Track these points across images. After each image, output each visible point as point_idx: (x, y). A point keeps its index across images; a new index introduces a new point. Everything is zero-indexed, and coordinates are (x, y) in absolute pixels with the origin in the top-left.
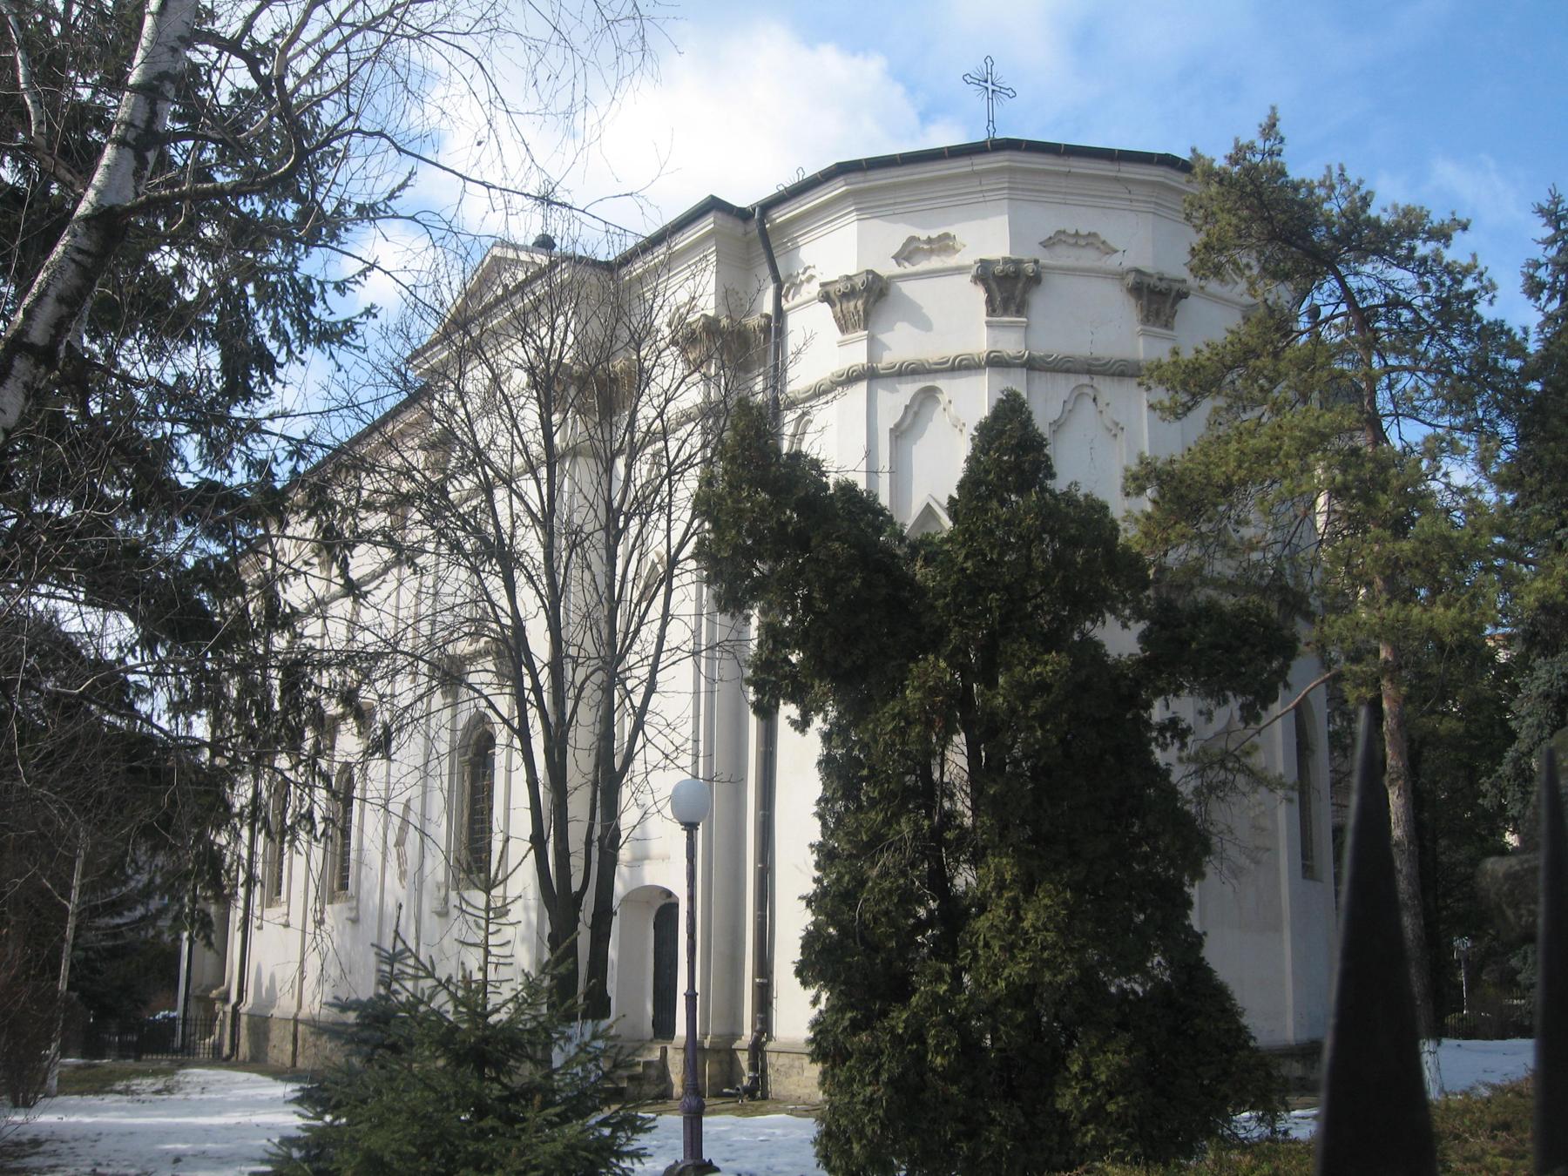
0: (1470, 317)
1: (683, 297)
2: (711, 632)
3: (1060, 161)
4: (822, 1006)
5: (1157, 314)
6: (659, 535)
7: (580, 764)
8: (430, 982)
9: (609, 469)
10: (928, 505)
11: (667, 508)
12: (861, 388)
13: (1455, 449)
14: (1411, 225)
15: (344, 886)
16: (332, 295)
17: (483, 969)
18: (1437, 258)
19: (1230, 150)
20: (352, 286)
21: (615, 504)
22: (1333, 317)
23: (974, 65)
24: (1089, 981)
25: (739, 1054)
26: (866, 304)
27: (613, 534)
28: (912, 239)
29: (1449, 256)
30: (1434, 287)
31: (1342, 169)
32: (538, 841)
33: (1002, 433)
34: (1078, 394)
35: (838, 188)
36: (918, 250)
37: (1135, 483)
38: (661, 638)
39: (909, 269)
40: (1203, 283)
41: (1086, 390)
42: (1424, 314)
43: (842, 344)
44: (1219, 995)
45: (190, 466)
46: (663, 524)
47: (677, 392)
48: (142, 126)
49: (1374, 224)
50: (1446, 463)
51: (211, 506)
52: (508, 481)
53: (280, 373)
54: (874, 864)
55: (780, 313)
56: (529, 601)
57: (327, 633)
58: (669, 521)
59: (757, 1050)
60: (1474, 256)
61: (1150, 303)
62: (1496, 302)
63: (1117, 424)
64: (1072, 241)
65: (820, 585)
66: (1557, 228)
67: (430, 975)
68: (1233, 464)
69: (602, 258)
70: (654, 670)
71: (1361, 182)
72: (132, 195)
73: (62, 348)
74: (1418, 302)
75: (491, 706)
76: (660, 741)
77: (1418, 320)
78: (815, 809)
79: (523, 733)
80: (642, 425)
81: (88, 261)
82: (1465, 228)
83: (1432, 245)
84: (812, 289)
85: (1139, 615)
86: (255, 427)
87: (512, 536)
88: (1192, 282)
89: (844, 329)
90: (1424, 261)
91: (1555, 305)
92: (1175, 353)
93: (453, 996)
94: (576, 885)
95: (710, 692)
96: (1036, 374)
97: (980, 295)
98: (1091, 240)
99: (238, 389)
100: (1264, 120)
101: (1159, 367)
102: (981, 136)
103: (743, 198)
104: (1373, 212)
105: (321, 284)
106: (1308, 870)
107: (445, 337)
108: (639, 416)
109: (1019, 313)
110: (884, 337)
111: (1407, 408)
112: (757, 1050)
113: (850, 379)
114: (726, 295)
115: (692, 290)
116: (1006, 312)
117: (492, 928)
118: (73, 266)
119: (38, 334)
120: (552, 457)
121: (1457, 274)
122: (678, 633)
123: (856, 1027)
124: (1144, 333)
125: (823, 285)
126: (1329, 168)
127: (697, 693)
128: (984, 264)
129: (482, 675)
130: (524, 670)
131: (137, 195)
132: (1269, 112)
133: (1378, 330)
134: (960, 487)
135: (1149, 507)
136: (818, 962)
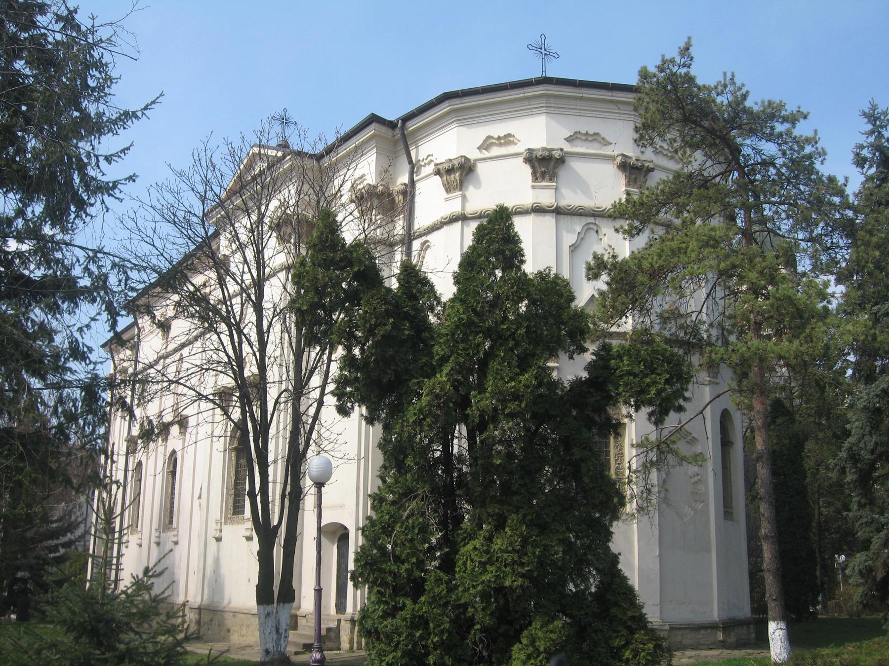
0: (811, 170)
3: (577, 90)
12: (458, 225)
14: (773, 112)
15: (171, 522)
16: (103, 163)
18: (789, 133)
19: (659, 62)
20: (116, 158)
23: (535, 39)
26: (461, 175)
28: (489, 137)
29: (796, 132)
31: (733, 75)
34: (587, 228)
35: (445, 108)
36: (492, 144)
39: (486, 154)
41: (592, 226)
42: (783, 170)
43: (447, 200)
49: (749, 112)
53: (89, 210)
55: (412, 183)
60: (816, 131)
61: (631, 174)
62: (825, 162)
64: (584, 138)
66: (874, 125)
71: (743, 85)
77: (779, 174)
78: (378, 473)
82: (805, 117)
83: (787, 126)
84: (431, 168)
89: (448, 190)
90: (780, 135)
91: (873, 170)
96: (562, 216)
97: (527, 170)
98: (594, 137)
100: (682, 45)
103: (391, 116)
104: (748, 103)
106: (727, 511)
109: (551, 180)
110: (467, 194)
115: (366, 169)
116: (543, 179)
121: (801, 143)
123: (385, 615)
125: (436, 165)
126: (725, 74)
128: (530, 151)
132: (686, 40)
134: (460, 265)
135: (605, 288)
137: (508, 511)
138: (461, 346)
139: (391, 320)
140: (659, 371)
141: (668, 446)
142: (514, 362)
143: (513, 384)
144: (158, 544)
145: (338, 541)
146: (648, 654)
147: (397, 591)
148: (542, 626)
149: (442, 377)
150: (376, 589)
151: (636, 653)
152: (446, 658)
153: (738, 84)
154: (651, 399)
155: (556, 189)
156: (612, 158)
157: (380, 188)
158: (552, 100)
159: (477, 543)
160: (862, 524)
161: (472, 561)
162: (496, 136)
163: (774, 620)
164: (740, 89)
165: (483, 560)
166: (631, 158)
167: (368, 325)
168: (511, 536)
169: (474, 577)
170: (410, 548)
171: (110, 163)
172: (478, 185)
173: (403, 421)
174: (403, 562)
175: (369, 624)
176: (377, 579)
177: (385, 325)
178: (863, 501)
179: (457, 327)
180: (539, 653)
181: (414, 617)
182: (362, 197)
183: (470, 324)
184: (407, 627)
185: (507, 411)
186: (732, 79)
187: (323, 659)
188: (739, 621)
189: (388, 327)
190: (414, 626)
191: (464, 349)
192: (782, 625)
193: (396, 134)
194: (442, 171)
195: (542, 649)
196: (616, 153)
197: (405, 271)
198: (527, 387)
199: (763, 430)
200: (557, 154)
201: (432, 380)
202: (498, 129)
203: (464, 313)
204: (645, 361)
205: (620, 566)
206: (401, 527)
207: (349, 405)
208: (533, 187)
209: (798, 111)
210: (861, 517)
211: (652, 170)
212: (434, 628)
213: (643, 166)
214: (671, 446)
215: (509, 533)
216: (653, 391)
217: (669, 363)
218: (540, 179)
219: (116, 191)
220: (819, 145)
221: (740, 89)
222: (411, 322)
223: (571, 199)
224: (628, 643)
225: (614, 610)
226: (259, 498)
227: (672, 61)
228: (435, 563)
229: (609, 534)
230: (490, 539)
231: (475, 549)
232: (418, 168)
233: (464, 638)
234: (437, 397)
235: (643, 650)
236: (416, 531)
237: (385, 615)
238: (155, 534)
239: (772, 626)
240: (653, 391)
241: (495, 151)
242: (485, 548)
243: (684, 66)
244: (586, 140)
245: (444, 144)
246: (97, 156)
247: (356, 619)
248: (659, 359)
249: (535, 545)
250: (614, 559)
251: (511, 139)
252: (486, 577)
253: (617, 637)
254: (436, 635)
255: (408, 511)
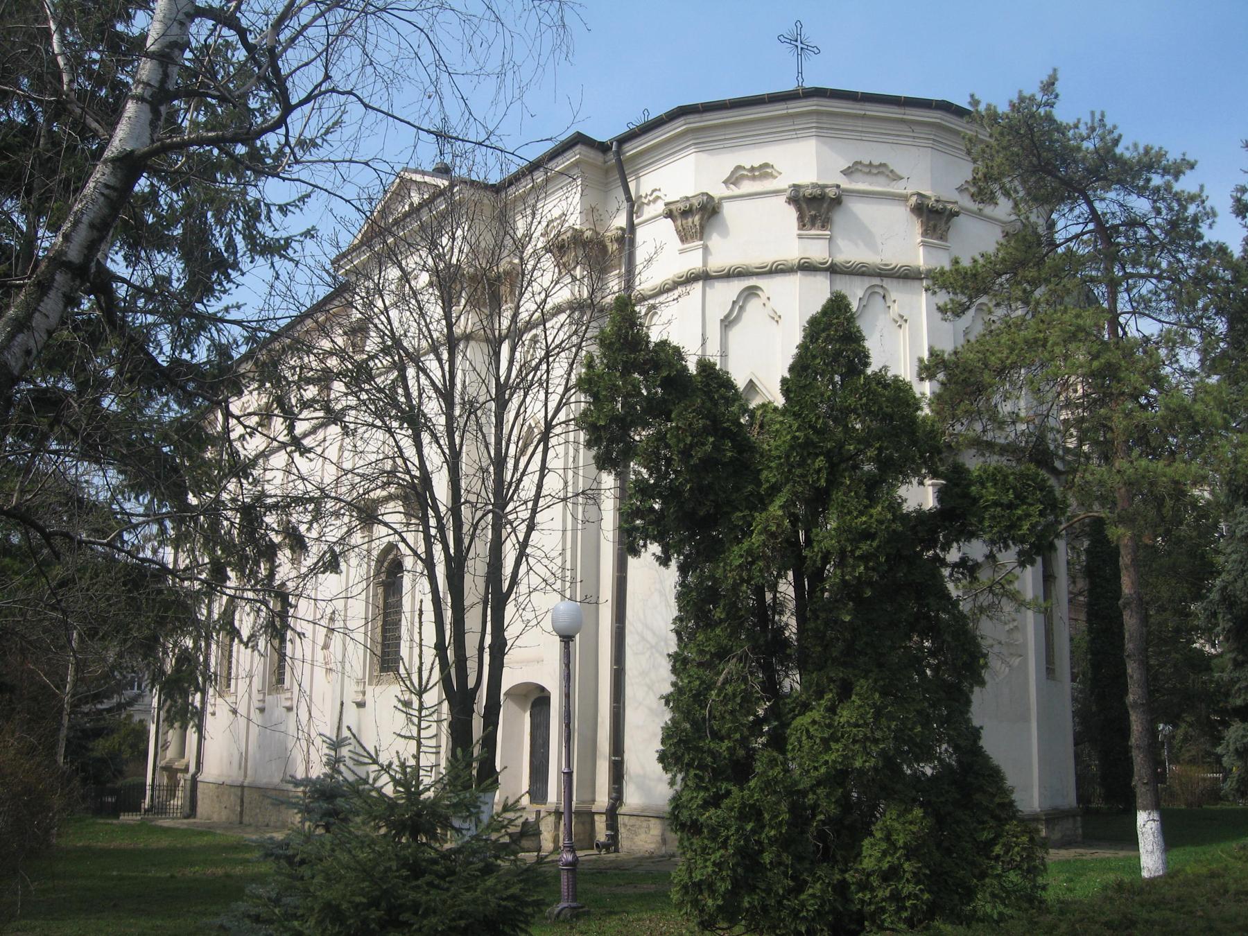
1: (556, 213)
2: (575, 483)
3: (858, 106)
4: (678, 787)
5: (935, 227)
6: (539, 405)
7: (474, 586)
8: (376, 767)
9: (497, 354)
10: (751, 381)
11: (545, 385)
12: (698, 286)
13: (1186, 341)
14: (1151, 162)
15: (281, 681)
16: (276, 215)
17: (417, 757)
18: (1168, 188)
21: (502, 379)
22: (1083, 234)
23: (787, 28)
24: (890, 764)
25: (597, 817)
26: (701, 219)
27: (502, 405)
28: (739, 168)
29: (1177, 187)
30: (1164, 212)
31: (1103, 115)
32: (440, 647)
33: (828, 326)
35: (678, 126)
36: (743, 177)
37: (926, 371)
38: (540, 486)
39: (735, 191)
40: (981, 206)
41: (877, 290)
42: (1157, 232)
43: (682, 252)
44: (995, 775)
45: (163, 349)
46: (542, 395)
47: (551, 286)
48: (157, 85)
49: (1118, 160)
50: (1181, 353)
51: (174, 378)
52: (415, 358)
54: (719, 674)
55: (632, 227)
56: (435, 458)
57: (275, 478)
58: (547, 393)
59: (612, 815)
60: (1202, 187)
61: (928, 220)
62: (1215, 226)
63: (902, 317)
65: (676, 444)
67: (375, 762)
68: (1006, 352)
69: (492, 182)
70: (534, 512)
71: (1115, 127)
72: (148, 141)
73: (93, 264)
74: (1151, 222)
75: (404, 540)
76: (538, 568)
78: (673, 627)
79: (429, 564)
80: (524, 315)
81: (114, 195)
82: (1192, 166)
84: (659, 207)
85: (935, 474)
86: (216, 319)
87: (420, 403)
88: (966, 202)
90: (1157, 190)
92: (956, 262)
93: (393, 778)
94: (471, 683)
95: (574, 530)
96: (838, 276)
97: (792, 213)
98: (879, 170)
99: (201, 286)
100: (1045, 79)
101: (942, 273)
102: (790, 86)
105: (268, 206)
106: (1050, 669)
107: (367, 241)
108: (522, 310)
109: (823, 227)
110: (710, 244)
111: (1142, 308)
112: (612, 815)
113: (690, 279)
114: (591, 212)
115: (564, 207)
116: (813, 225)
117: (424, 724)
118: (102, 199)
119: (74, 254)
120: (452, 342)
121: (1183, 200)
122: (553, 484)
123: (706, 805)
124: (924, 244)
125: (667, 204)
126: (1093, 113)
127: (564, 531)
128: (796, 187)
129: (393, 514)
130: (430, 512)
131: (153, 141)
133: (1119, 244)
134: (791, 369)
136: (678, 750)
137: (855, 676)
138: (798, 471)
139: (711, 439)
140: (1029, 501)
141: (1003, 587)
142: (862, 492)
143: (864, 519)
144: (262, 710)
145: (532, 707)
146: (1024, 849)
147: (717, 774)
148: (899, 816)
149: (775, 509)
150: (692, 772)
151: (1008, 848)
152: (784, 855)
153: (1109, 126)
154: (1024, 535)
155: (830, 239)
156: (904, 198)
157: (588, 234)
158: (825, 119)
159: (815, 715)
160: (1240, 689)
161: (810, 737)
162: (748, 167)
163: (1145, 809)
164: (1111, 132)
165: (826, 735)
166: (929, 198)
167: (682, 445)
168: (860, 706)
169: (815, 758)
170: (732, 722)
171: (285, 215)
172: (725, 233)
173: (726, 564)
174: (722, 739)
175: (684, 816)
176: (693, 760)
177: (703, 444)
178: (1240, 658)
179: (792, 448)
180: (896, 849)
181: (744, 805)
182: (563, 246)
183: (808, 443)
184: (737, 819)
185: (858, 553)
186: (1101, 120)
187: (576, 860)
188: (1063, 811)
189: (709, 448)
190: (743, 817)
191: (802, 476)
192: (1155, 815)
193: (609, 161)
194: (675, 213)
195: (901, 843)
196: (909, 191)
197: (704, 371)
198: (880, 522)
199: (1132, 569)
200: (831, 193)
201: (764, 515)
202: (751, 157)
203: (798, 429)
204: (1014, 488)
205: (981, 743)
206: (718, 695)
207: (641, 543)
208: (800, 237)
209: (1183, 160)
210: (1239, 679)
211: (957, 214)
212: (770, 820)
213: (945, 209)
214: (1007, 587)
215: (858, 702)
216: (1026, 526)
217: (1041, 490)
218: (808, 226)
219: (290, 251)
220: (1207, 204)
221: (1111, 132)
222: (733, 441)
223: (850, 252)
224: (998, 836)
225: (978, 796)
226: (450, 653)
227: (1032, 98)
228: (763, 740)
229: (968, 702)
230: (832, 710)
231: (814, 722)
232: (639, 207)
233: (803, 832)
234: (773, 535)
235: (1017, 845)
236: (738, 700)
237: (706, 805)
238: (256, 696)
239: (1142, 817)
240: (1026, 526)
241: (747, 187)
242: (827, 721)
243: (1046, 104)
244: (869, 173)
245: (675, 176)
246: (268, 206)
247: (562, 810)
248: (1030, 486)
249: (891, 717)
250: (976, 733)
251: (769, 170)
252: (830, 757)
253: (984, 829)
254: (773, 828)
255: (723, 676)
